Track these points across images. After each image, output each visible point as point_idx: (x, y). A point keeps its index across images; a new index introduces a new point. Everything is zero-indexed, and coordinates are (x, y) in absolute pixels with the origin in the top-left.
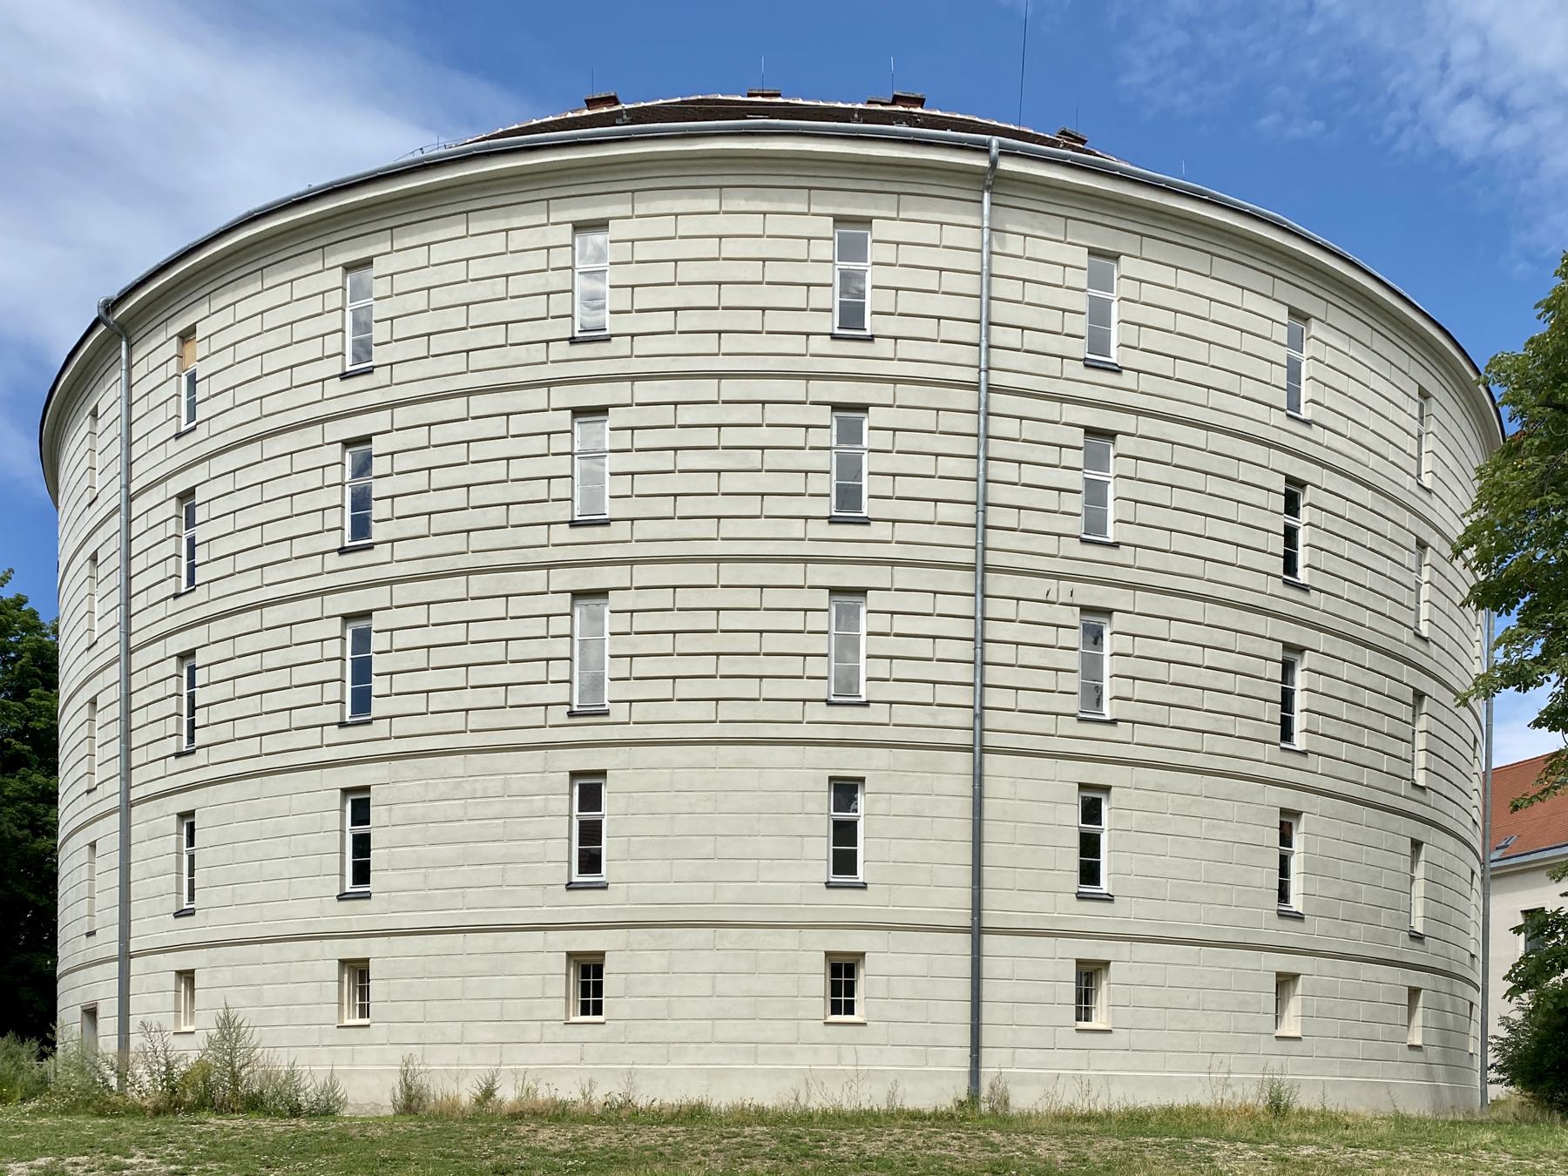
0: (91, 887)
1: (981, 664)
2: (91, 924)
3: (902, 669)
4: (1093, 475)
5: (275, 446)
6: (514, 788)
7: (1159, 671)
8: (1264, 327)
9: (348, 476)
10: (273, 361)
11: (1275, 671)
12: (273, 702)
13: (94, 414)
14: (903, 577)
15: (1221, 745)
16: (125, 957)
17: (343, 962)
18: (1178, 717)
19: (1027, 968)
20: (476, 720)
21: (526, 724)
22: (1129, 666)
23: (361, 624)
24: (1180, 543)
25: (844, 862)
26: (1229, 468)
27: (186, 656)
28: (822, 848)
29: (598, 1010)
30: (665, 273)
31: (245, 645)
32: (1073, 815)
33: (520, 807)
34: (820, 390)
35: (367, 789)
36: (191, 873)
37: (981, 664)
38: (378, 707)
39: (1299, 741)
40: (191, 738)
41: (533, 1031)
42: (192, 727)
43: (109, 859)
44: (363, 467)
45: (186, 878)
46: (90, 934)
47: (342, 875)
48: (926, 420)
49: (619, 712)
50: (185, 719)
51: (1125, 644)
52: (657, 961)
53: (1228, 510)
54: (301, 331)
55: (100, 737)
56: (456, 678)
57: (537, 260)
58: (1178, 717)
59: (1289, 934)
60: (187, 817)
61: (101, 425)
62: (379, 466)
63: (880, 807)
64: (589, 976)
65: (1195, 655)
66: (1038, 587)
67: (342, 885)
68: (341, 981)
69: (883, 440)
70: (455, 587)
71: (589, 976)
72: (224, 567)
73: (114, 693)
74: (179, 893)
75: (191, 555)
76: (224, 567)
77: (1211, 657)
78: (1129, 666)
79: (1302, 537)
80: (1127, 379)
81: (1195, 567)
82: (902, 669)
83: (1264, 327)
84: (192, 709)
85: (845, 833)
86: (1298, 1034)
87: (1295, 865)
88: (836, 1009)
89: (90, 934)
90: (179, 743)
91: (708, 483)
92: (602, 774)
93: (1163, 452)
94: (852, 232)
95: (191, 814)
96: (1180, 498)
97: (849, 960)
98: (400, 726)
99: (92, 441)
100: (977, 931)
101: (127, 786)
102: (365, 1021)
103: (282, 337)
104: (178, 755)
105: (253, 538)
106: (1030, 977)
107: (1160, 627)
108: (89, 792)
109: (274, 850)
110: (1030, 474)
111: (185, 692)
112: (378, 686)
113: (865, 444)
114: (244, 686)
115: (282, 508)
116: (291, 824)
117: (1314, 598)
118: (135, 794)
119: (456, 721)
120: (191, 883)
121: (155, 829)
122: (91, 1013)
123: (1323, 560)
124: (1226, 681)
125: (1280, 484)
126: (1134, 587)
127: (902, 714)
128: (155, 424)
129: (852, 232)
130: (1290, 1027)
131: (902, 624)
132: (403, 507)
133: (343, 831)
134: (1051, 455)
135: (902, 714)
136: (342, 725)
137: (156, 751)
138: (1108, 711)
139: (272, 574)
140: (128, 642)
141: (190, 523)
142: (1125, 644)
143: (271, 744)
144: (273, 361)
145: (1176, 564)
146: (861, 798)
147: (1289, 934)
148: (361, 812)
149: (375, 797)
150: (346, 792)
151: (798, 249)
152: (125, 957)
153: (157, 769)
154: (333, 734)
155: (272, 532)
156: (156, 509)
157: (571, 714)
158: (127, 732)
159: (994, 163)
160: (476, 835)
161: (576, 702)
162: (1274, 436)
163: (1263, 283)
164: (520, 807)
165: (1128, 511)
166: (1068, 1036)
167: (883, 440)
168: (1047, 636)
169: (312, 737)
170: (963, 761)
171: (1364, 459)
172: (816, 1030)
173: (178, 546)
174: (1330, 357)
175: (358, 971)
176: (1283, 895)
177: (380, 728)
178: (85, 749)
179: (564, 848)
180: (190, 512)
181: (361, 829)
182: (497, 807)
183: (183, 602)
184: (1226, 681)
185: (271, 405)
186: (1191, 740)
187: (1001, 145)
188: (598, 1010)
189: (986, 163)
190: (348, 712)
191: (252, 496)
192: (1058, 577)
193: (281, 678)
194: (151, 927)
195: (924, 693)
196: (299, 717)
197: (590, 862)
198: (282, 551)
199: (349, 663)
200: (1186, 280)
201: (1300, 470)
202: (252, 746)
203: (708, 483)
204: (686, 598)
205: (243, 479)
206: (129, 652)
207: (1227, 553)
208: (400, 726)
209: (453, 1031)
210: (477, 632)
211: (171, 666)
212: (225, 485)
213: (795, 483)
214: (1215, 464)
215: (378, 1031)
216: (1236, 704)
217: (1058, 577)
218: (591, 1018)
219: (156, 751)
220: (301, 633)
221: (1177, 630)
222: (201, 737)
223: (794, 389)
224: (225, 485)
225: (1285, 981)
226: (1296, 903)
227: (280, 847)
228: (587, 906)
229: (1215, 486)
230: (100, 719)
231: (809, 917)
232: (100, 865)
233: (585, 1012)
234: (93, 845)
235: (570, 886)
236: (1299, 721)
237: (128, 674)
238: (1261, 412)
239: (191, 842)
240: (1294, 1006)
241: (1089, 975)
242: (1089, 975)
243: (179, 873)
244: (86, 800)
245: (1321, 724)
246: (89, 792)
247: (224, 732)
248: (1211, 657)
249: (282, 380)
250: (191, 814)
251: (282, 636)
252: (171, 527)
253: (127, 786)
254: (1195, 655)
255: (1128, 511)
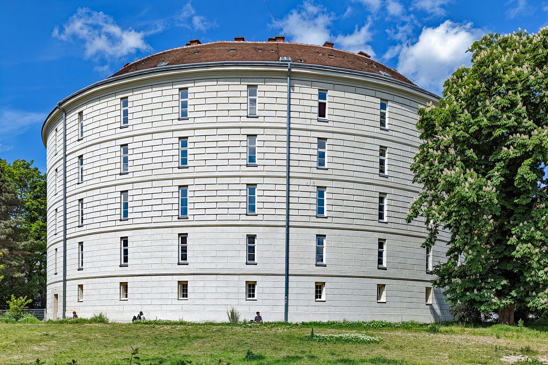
0: (56, 261)
1: (288, 203)
2: (56, 271)
3: (266, 205)
4: (320, 150)
5: (103, 145)
6: (164, 238)
7: (340, 203)
8: (372, 105)
9: (122, 154)
10: (103, 123)
11: (377, 200)
12: (103, 213)
13: (56, 130)
14: (267, 180)
15: (359, 222)
16: (65, 281)
17: (121, 283)
18: (346, 215)
19: (301, 285)
20: (154, 220)
21: (166, 221)
22: (331, 202)
23: (184, 188)
24: (346, 167)
25: (251, 257)
26: (362, 145)
27: (81, 200)
28: (244, 254)
29: (187, 297)
30: (203, 101)
31: (96, 198)
32: (314, 244)
33: (166, 243)
34: (244, 131)
35: (127, 237)
36: (82, 258)
37: (288, 203)
38: (130, 216)
39: (386, 219)
40: (82, 222)
41: (169, 302)
42: (82, 219)
43: (61, 254)
44: (126, 152)
45: (81, 260)
46: (56, 274)
47: (121, 260)
48: (273, 138)
49: (191, 218)
50: (81, 217)
51: (330, 196)
52: (201, 284)
53: (362, 157)
54: (110, 115)
55: (58, 220)
56: (149, 208)
57: (170, 98)
58: (346, 215)
59: (381, 273)
60: (81, 243)
61: (58, 134)
62: (130, 152)
63: (261, 243)
64: (184, 287)
65: (351, 198)
66: (305, 182)
67: (121, 263)
68: (120, 288)
69: (261, 144)
70: (149, 184)
71: (184, 287)
72: (91, 177)
73: (62, 167)
74: (79, 264)
75: (82, 173)
76: (91, 177)
77: (356, 198)
78: (331, 202)
79: (386, 162)
80: (330, 124)
81: (351, 174)
82: (266, 205)
83: (372, 105)
84: (82, 214)
85: (251, 250)
86: (385, 301)
87: (384, 254)
88: (250, 296)
89: (56, 274)
90: (79, 223)
91: (214, 156)
92: (187, 234)
93: (341, 143)
94: (252, 90)
95: (82, 243)
96: (346, 155)
97: (253, 283)
98: (135, 221)
99: (56, 137)
100: (287, 275)
101: (65, 234)
102: (127, 299)
103: (105, 116)
104: (79, 227)
105: (98, 169)
106: (303, 288)
107: (341, 191)
108: (55, 234)
109: (102, 253)
110: (302, 151)
111: (81, 209)
112: (130, 210)
113: (256, 145)
114: (96, 209)
115: (105, 162)
116: (107, 247)
117: (390, 179)
118: (67, 236)
119: (149, 220)
120: (82, 261)
121: (73, 245)
122: (56, 296)
123: (392, 168)
124: (361, 204)
125: (378, 148)
126: (333, 180)
127: (266, 217)
128: (72, 136)
129: (252, 90)
130: (383, 299)
131: (266, 193)
132: (136, 163)
133: (121, 248)
134: (307, 146)
135: (266, 217)
136: (121, 220)
137: (73, 225)
138: (326, 214)
139: (103, 180)
140: (65, 195)
141: (82, 164)
142: (330, 196)
143: (103, 225)
144: (103, 123)
145: (345, 173)
146: (256, 241)
147: (381, 273)
148: (126, 243)
149: (129, 239)
150: (122, 238)
151: (238, 94)
152: (65, 281)
153: (73, 230)
154: (118, 223)
155: (103, 168)
156: (73, 160)
157: (179, 218)
158: (65, 219)
159: (289, 70)
160: (154, 250)
161: (180, 215)
162: (376, 135)
163: (373, 93)
164: (166, 243)
165: (331, 160)
166: (313, 302)
167: (261, 144)
168: (307, 195)
169: (113, 223)
170: (284, 230)
171: (408, 138)
172: (244, 302)
173: (79, 170)
174: (394, 110)
175: (124, 286)
176: (380, 262)
177: (130, 221)
178: (54, 222)
179: (175, 254)
180: (82, 161)
181: (126, 248)
182: (160, 243)
183: (80, 185)
184: (361, 204)
185: (102, 134)
186: (350, 221)
187: (291, 64)
188: (187, 297)
189: (287, 70)
190: (180, 115)
191: (97, 158)
192: (310, 179)
193: (105, 207)
194: (72, 272)
195: (273, 211)
196: (110, 218)
197: (184, 257)
198: (105, 174)
199: (122, 204)
200: (348, 95)
201: (384, 143)
202: (98, 225)
203: (214, 156)
204: (208, 187)
205: (95, 153)
206: (66, 156)
207: (362, 169)
208: (135, 221)
209: (149, 302)
210: (155, 196)
211: (77, 203)
212: (91, 155)
213: (237, 156)
214: (357, 145)
215: (130, 302)
216: (364, 211)
217: (310, 179)
218: (185, 298)
219: (73, 225)
220: (110, 196)
221: (345, 191)
222: (85, 222)
223: (237, 131)
224: (91, 155)
225: (381, 288)
226: (385, 265)
227: (105, 253)
228: (183, 269)
229: (356, 151)
230: (58, 215)
231: (241, 272)
232: (58, 255)
233: (183, 297)
234: (56, 249)
235: (179, 264)
236: (386, 214)
237: (65, 162)
238: (372, 129)
239: (82, 250)
240: (384, 293)
241: (319, 288)
242: (319, 288)
243: (79, 258)
244: (55, 237)
245: (392, 214)
246: (55, 234)
247: (91, 221)
248: (356, 198)
249: (105, 128)
250: (82, 243)
251: (105, 196)
252: (77, 165)
253: (65, 234)
254: (351, 198)
255: (331, 160)
